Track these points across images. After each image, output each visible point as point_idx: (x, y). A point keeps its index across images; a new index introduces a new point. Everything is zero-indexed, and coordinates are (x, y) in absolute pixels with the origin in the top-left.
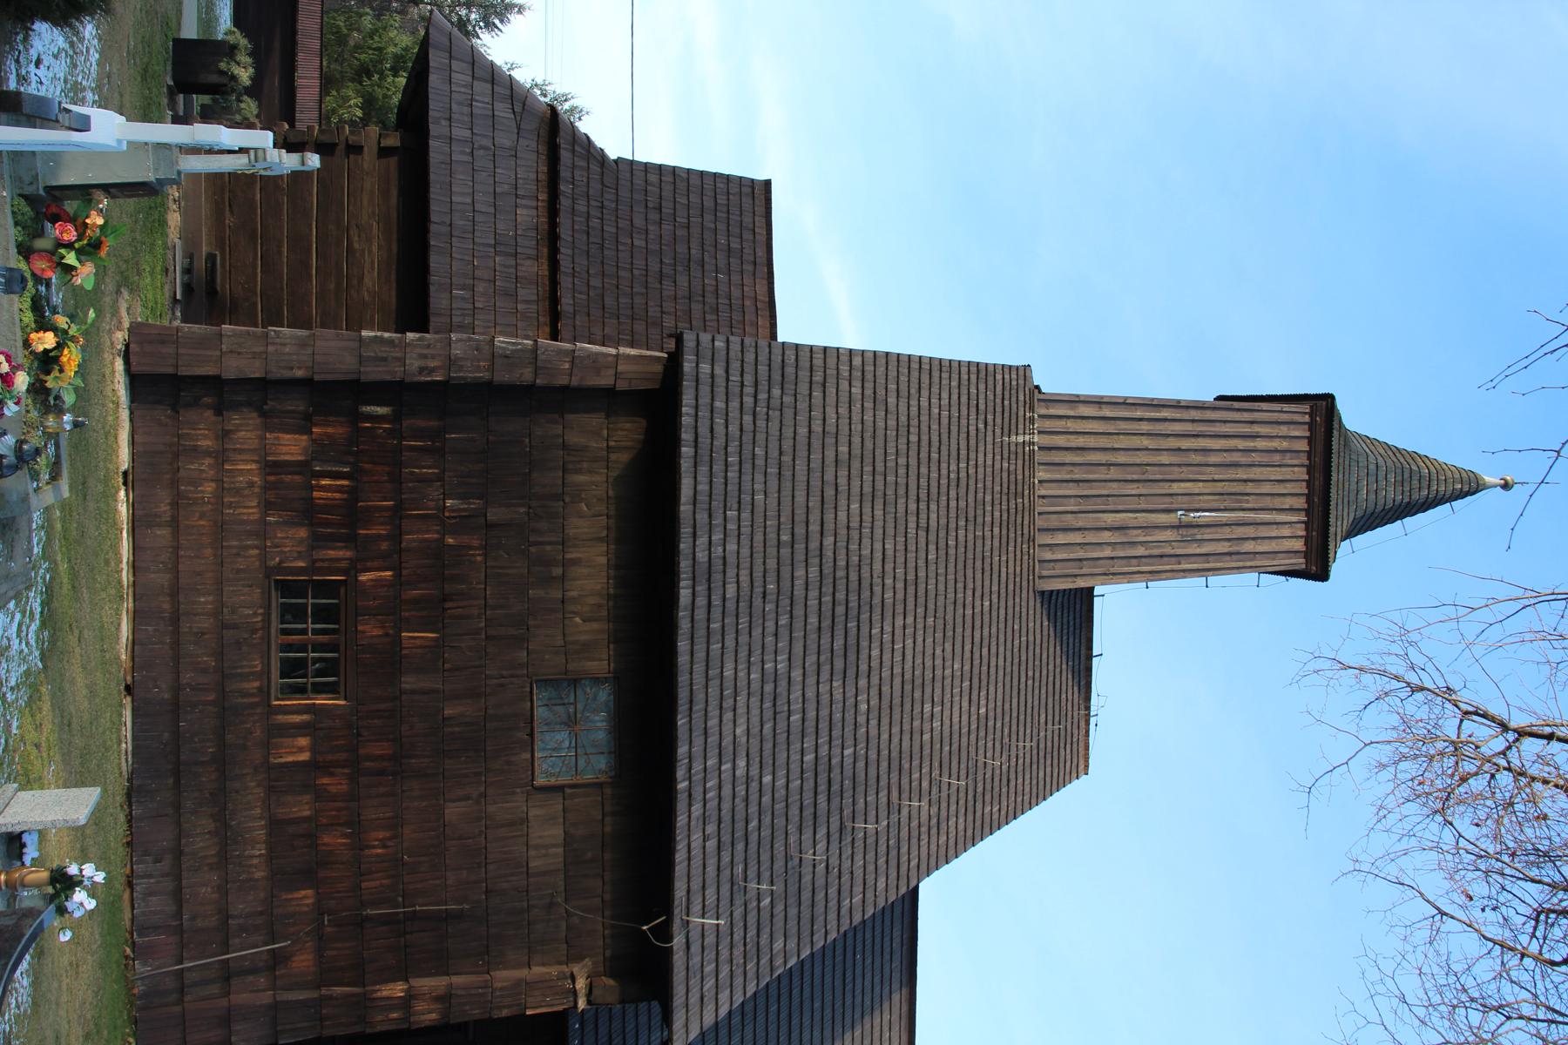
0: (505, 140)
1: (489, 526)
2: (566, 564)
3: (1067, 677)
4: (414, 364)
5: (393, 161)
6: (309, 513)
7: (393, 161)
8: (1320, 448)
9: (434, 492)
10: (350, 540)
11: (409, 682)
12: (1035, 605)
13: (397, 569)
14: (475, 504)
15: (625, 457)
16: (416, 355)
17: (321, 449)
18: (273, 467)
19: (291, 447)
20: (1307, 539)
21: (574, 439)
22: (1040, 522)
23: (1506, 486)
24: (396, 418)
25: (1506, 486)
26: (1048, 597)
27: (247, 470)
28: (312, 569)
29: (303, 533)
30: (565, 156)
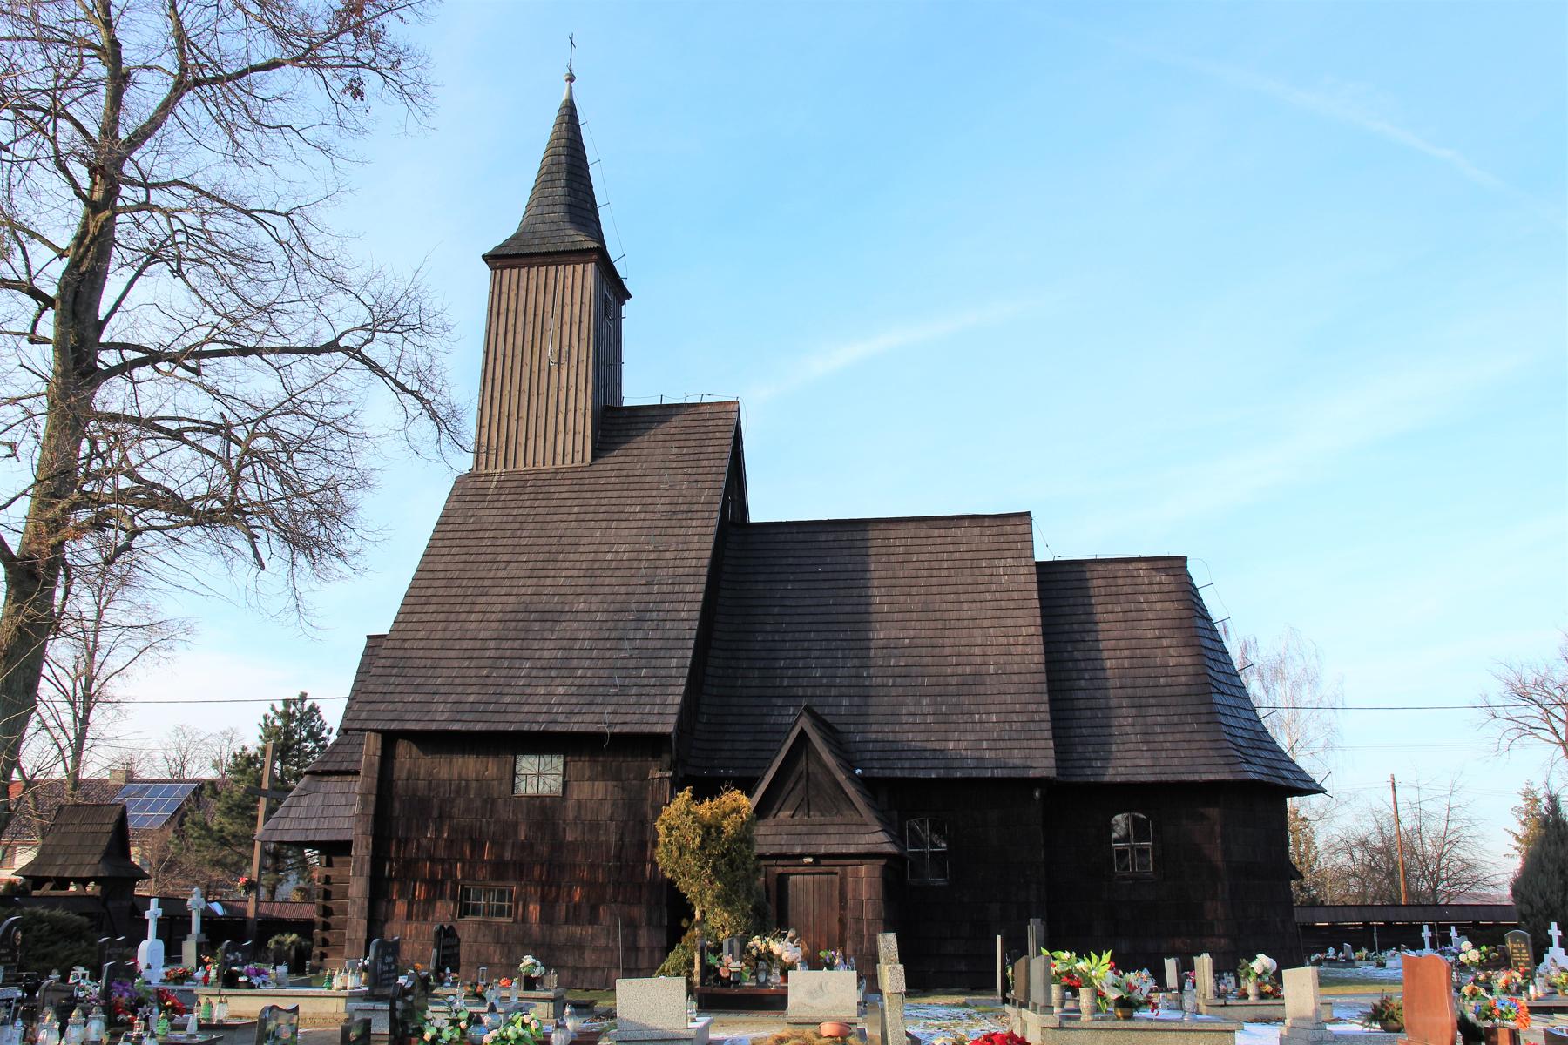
0: (319, 800)
1: (440, 816)
2: (460, 779)
3: (659, 432)
4: (364, 851)
5: (334, 859)
6: (430, 902)
7: (334, 859)
8: (516, 261)
9: (424, 842)
10: (443, 882)
11: (508, 855)
12: (613, 460)
13: (457, 861)
14: (431, 824)
15: (414, 749)
16: (362, 851)
17: (402, 895)
18: (409, 917)
19: (401, 908)
20: (576, 263)
21: (404, 775)
22: (540, 466)
23: (571, 79)
24: (391, 860)
25: (571, 79)
26: (601, 448)
27: (410, 928)
28: (453, 898)
29: (438, 904)
30: (328, 767)
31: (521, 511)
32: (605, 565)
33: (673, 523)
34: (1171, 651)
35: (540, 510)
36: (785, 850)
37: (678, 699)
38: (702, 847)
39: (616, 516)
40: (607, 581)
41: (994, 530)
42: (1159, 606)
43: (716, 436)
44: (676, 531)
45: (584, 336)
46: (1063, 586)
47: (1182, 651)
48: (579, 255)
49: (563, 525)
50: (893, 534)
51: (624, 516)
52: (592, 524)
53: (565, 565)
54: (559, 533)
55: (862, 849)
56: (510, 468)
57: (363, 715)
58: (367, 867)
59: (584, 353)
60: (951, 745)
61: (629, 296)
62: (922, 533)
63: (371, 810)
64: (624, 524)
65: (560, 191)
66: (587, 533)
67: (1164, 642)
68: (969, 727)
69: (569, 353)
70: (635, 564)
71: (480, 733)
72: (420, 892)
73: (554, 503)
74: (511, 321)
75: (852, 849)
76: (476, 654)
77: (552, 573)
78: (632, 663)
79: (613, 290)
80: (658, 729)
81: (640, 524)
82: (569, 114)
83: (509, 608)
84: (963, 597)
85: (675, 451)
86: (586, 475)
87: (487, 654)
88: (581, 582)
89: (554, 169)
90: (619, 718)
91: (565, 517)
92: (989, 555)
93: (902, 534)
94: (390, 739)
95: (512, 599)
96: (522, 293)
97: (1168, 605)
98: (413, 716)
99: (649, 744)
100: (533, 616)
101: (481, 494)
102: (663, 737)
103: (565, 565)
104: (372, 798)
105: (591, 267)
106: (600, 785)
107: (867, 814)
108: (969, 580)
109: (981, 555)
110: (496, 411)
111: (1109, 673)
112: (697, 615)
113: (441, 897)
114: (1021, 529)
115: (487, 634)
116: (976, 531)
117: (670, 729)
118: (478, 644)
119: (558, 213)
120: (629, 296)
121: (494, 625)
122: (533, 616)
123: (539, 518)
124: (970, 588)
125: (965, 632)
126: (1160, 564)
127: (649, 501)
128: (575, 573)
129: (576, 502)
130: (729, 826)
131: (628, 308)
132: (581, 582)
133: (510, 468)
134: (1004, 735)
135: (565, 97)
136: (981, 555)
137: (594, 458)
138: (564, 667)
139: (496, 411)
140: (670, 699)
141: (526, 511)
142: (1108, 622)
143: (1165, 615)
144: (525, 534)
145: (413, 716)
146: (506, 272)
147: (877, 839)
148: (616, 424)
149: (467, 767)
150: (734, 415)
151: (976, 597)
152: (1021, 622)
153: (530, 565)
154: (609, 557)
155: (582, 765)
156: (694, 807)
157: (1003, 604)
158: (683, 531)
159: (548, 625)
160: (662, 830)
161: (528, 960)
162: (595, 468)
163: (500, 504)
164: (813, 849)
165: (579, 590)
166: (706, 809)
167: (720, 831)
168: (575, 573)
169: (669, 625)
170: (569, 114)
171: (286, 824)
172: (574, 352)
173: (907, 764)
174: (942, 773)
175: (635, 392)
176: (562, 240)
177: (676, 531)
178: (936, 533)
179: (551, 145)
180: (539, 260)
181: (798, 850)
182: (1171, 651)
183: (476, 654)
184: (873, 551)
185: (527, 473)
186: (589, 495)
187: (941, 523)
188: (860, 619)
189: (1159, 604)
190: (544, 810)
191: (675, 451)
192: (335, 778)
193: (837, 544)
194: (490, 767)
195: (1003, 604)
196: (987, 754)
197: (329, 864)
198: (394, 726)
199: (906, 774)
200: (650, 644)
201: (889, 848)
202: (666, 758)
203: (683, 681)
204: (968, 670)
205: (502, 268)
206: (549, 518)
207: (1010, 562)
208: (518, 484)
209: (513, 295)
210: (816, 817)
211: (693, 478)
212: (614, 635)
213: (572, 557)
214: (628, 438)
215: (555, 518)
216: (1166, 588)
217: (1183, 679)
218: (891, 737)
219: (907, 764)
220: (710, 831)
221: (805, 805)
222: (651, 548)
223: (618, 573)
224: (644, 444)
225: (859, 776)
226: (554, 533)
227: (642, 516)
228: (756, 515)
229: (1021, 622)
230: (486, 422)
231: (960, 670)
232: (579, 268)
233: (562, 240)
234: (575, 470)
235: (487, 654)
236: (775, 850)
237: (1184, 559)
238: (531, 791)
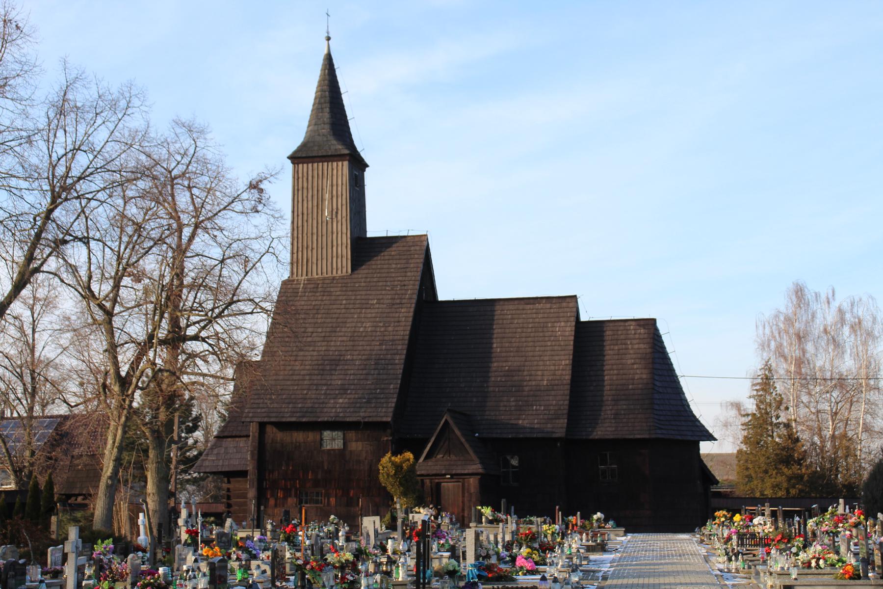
6: (285, 498)
11: (319, 477)
12: (363, 271)
16: (252, 476)
17: (272, 496)
18: (276, 506)
19: (272, 502)
23: (329, 39)
25: (329, 39)
26: (356, 264)
28: (296, 496)
30: (226, 434)
31: (317, 303)
32: (359, 334)
33: (393, 310)
34: (638, 371)
35: (326, 302)
36: (438, 472)
37: (393, 405)
38: (395, 474)
39: (364, 306)
40: (361, 343)
41: (558, 305)
42: (636, 346)
43: (415, 254)
44: (394, 315)
45: (344, 202)
46: (590, 337)
47: (643, 371)
48: (339, 157)
49: (338, 311)
50: (506, 307)
51: (368, 306)
52: (352, 311)
53: (340, 334)
54: (336, 316)
55: (470, 471)
56: (309, 276)
57: (251, 415)
58: (255, 483)
59: (344, 213)
60: (520, 422)
61: (368, 166)
62: (521, 307)
63: (256, 457)
64: (368, 311)
65: (326, 115)
66: (350, 316)
67: (635, 366)
68: (530, 412)
69: (337, 213)
70: (374, 334)
71: (305, 422)
72: (280, 494)
73: (333, 298)
74: (305, 194)
75: (466, 472)
76: (301, 382)
77: (334, 339)
78: (373, 387)
79: (358, 165)
80: (384, 419)
81: (376, 310)
82: (329, 59)
83: (314, 358)
84: (537, 344)
85: (394, 266)
86: (349, 281)
87: (306, 382)
88: (348, 343)
89: (323, 101)
90: (367, 414)
91: (339, 306)
92: (553, 320)
93: (511, 307)
94: (262, 426)
95: (315, 353)
96: (310, 178)
97: (642, 346)
98: (274, 415)
99: (381, 426)
100: (326, 362)
101: (295, 292)
102: (387, 423)
103: (340, 334)
104: (256, 452)
105: (346, 163)
106: (360, 444)
107: (473, 455)
108: (541, 334)
109: (548, 320)
110: (300, 245)
111: (606, 383)
112: (403, 361)
113: (290, 496)
114: (571, 305)
115: (305, 372)
116: (548, 306)
117: (389, 419)
118: (301, 377)
119: (326, 129)
120: (368, 166)
121: (307, 367)
122: (326, 362)
123: (326, 307)
124: (541, 339)
125: (535, 363)
126: (642, 323)
127: (381, 297)
128: (345, 339)
129: (344, 297)
130: (405, 466)
131: (368, 174)
132: (348, 343)
133: (309, 276)
134: (542, 415)
135: (326, 52)
136: (548, 320)
137: (353, 270)
138: (344, 390)
139: (300, 245)
140: (390, 405)
141: (319, 303)
142: (610, 352)
143: (638, 351)
144: (320, 316)
145: (274, 415)
146: (300, 166)
147: (477, 467)
148: (365, 249)
149: (299, 436)
150: (425, 243)
151: (543, 343)
152: (562, 357)
153: (323, 334)
154: (361, 329)
155: (351, 435)
156: (393, 458)
157: (556, 348)
158: (397, 315)
159: (333, 367)
160: (381, 468)
161: (332, 517)
162: (353, 276)
163: (305, 298)
164: (450, 472)
165: (347, 348)
166: (397, 459)
167: (402, 468)
168: (345, 339)
169: (390, 367)
170: (329, 59)
171: (207, 463)
172: (340, 212)
173: (499, 431)
174: (514, 435)
175: (374, 229)
176: (331, 144)
177: (394, 315)
178: (528, 307)
179: (319, 82)
180: (318, 159)
181: (443, 472)
182: (638, 371)
183: (301, 382)
184: (496, 317)
185: (318, 279)
186: (350, 293)
187: (532, 301)
188: (486, 355)
189: (639, 346)
190: (341, 454)
191: (394, 266)
192: (229, 439)
193: (480, 312)
194: (311, 436)
195: (556, 348)
196: (536, 426)
197: (229, 482)
198: (266, 420)
199: (498, 436)
200: (381, 377)
201: (481, 471)
202: (389, 431)
203: (395, 396)
204: (534, 383)
205: (298, 164)
206: (331, 307)
207: (563, 324)
208: (314, 286)
209: (305, 179)
210: (453, 457)
211: (403, 283)
212: (364, 372)
213: (343, 330)
214: (370, 258)
215: (334, 306)
216: (642, 336)
217: (640, 386)
218: (494, 418)
219: (499, 431)
220: (398, 467)
221: (449, 452)
222: (381, 324)
223: (366, 339)
224: (378, 262)
225: (477, 437)
226: (334, 316)
227: (377, 306)
228: (444, 294)
229: (562, 357)
230: (295, 251)
231: (530, 383)
232: (340, 163)
233: (331, 144)
234: (342, 278)
235: (306, 382)
236: (434, 472)
237: (654, 320)
238: (328, 447)
